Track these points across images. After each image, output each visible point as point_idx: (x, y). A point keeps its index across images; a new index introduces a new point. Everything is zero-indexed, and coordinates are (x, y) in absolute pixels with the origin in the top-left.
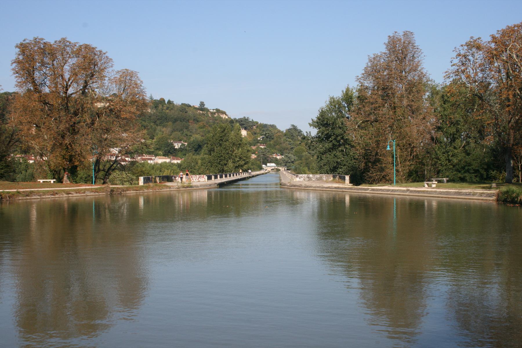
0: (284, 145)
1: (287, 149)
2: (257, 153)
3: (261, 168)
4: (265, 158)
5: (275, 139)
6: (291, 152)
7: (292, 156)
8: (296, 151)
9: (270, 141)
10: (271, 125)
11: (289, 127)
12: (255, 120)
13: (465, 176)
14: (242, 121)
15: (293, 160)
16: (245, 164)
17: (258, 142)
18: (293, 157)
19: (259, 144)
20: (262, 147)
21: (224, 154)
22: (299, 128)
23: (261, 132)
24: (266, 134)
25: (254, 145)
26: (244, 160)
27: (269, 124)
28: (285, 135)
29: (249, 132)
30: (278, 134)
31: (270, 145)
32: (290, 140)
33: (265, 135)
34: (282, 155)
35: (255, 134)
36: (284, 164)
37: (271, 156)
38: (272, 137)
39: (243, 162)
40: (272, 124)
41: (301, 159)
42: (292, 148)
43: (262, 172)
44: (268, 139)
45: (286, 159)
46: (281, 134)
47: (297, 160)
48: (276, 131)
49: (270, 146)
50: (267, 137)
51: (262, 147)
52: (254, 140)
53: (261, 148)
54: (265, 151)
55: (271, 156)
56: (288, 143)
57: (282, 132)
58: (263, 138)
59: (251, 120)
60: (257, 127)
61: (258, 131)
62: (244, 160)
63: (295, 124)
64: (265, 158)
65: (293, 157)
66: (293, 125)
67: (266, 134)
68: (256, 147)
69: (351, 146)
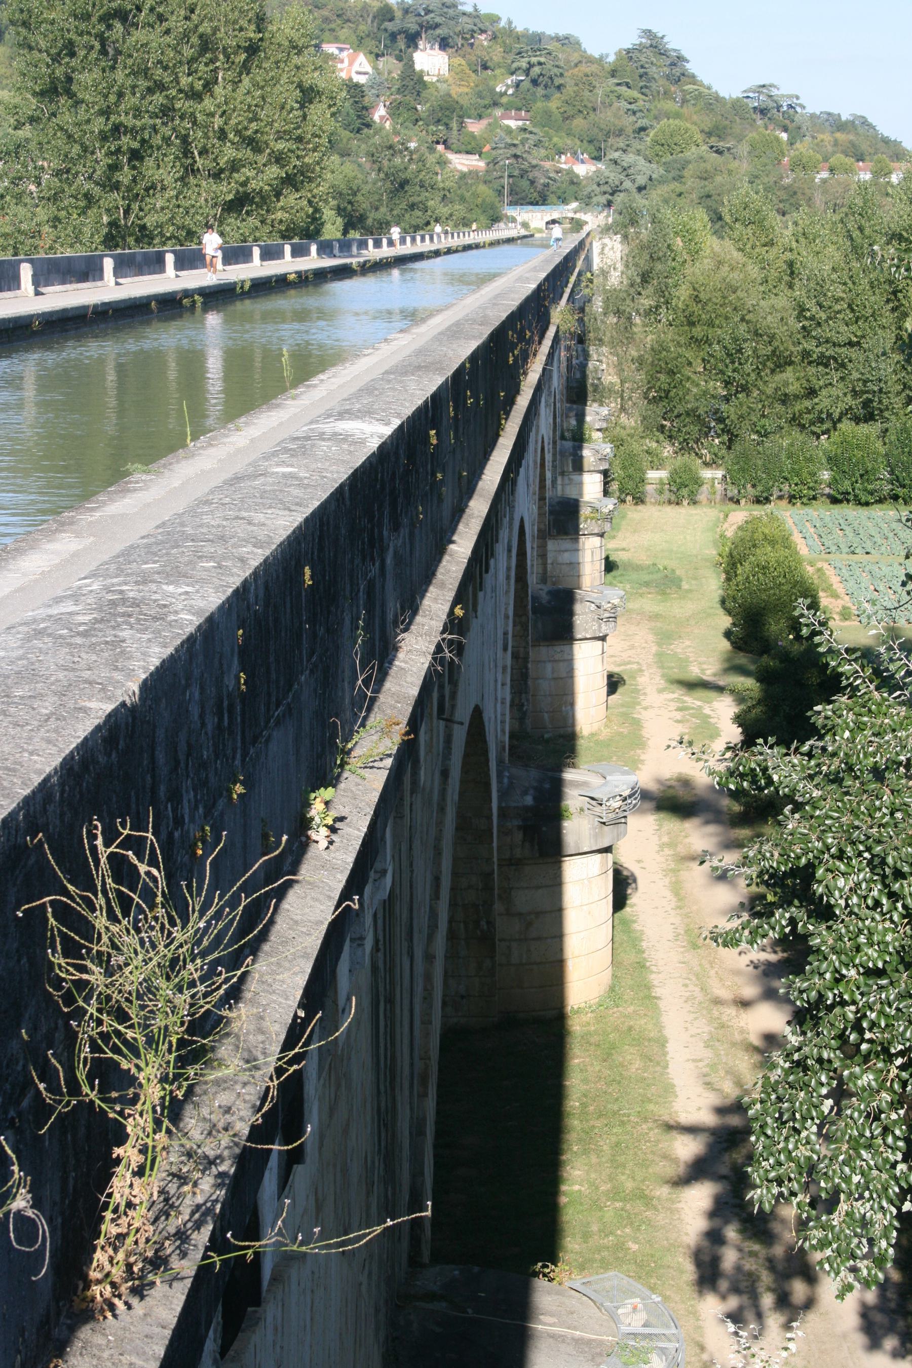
0: (606, 117)
1: (620, 132)
2: (487, 148)
3: (495, 219)
4: (523, 174)
5: (570, 90)
6: (636, 145)
7: (641, 161)
8: (656, 142)
9: (547, 97)
10: (557, 39)
11: (630, 39)
12: (484, 10)
13: (244, 184)
14: (428, 11)
15: (641, 180)
16: (290, 181)
17: (496, 104)
18: (644, 169)
19: (498, 112)
20: (513, 124)
21: (137, 113)
22: (673, 43)
23: (512, 56)
24: (531, 65)
25: (480, 117)
26: (279, 159)
27: (550, 31)
28: (613, 73)
29: (458, 60)
30: (584, 68)
31: (548, 114)
32: (635, 94)
33: (527, 72)
34: (597, 158)
35: (485, 67)
36: (603, 199)
37: (547, 165)
38: (558, 81)
39: (274, 171)
40: (562, 33)
41: (679, 178)
42: (643, 129)
43: (503, 231)
44: (540, 91)
45: (614, 177)
46: (594, 68)
47: (662, 181)
48: (575, 57)
49: (546, 120)
50: (535, 82)
51: (513, 124)
52: (480, 95)
53: (509, 130)
54: (523, 143)
55: (547, 165)
56: (624, 105)
57: (600, 61)
58: (518, 85)
59: (469, 9)
60: (494, 38)
61: (496, 54)
62: (279, 159)
63: (659, 30)
64: (523, 174)
65: (644, 169)
66: (648, 33)
67: (531, 65)
68: (484, 122)
69: (877, 673)
